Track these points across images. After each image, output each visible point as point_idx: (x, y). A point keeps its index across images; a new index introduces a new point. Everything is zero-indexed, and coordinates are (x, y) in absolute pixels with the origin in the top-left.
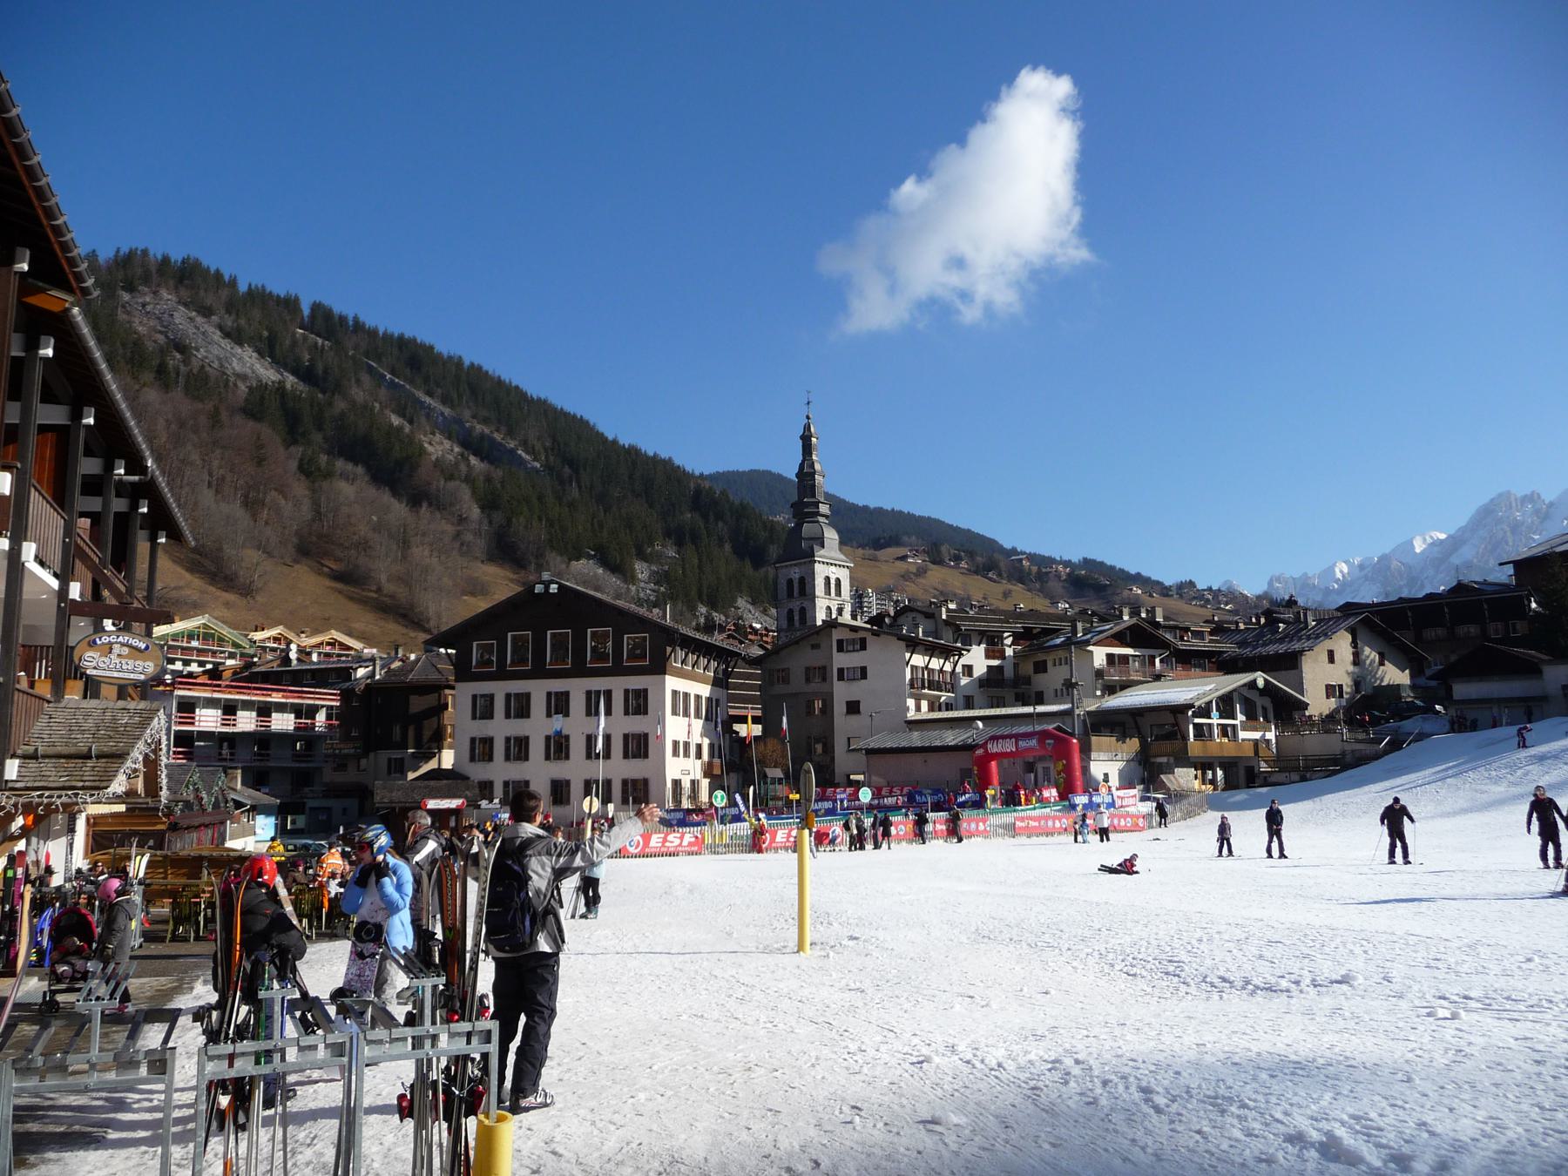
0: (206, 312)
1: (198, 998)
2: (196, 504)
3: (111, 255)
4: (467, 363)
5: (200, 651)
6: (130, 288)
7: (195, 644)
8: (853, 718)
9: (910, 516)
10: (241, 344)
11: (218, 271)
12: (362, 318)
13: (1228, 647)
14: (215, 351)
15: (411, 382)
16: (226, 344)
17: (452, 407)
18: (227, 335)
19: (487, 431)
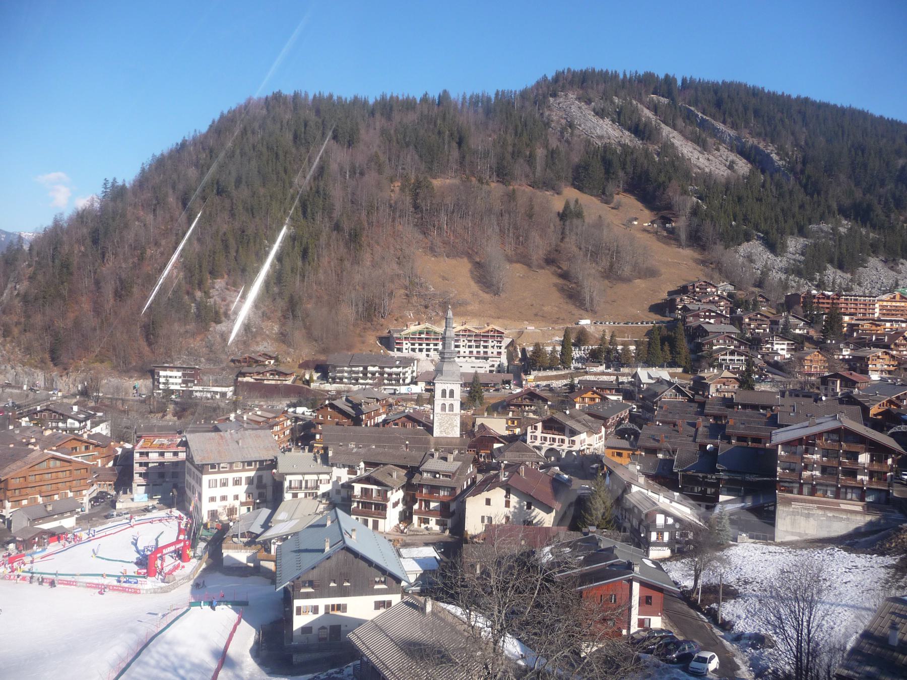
0: (588, 102)
1: (851, 594)
2: (233, 215)
3: (554, 74)
4: (766, 91)
5: (427, 339)
6: (554, 95)
7: (423, 336)
8: (213, 503)
9: (755, 93)
10: (602, 118)
11: (667, 76)
12: (694, 77)
13: (874, 529)
14: (589, 124)
15: (714, 118)
16: (595, 119)
17: (737, 129)
18: (597, 114)
19: (756, 142)
